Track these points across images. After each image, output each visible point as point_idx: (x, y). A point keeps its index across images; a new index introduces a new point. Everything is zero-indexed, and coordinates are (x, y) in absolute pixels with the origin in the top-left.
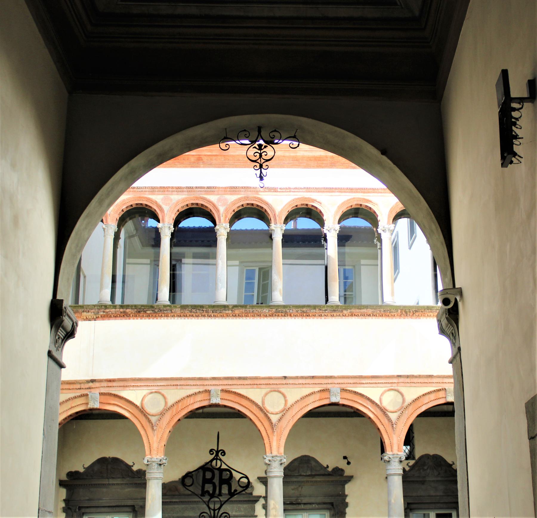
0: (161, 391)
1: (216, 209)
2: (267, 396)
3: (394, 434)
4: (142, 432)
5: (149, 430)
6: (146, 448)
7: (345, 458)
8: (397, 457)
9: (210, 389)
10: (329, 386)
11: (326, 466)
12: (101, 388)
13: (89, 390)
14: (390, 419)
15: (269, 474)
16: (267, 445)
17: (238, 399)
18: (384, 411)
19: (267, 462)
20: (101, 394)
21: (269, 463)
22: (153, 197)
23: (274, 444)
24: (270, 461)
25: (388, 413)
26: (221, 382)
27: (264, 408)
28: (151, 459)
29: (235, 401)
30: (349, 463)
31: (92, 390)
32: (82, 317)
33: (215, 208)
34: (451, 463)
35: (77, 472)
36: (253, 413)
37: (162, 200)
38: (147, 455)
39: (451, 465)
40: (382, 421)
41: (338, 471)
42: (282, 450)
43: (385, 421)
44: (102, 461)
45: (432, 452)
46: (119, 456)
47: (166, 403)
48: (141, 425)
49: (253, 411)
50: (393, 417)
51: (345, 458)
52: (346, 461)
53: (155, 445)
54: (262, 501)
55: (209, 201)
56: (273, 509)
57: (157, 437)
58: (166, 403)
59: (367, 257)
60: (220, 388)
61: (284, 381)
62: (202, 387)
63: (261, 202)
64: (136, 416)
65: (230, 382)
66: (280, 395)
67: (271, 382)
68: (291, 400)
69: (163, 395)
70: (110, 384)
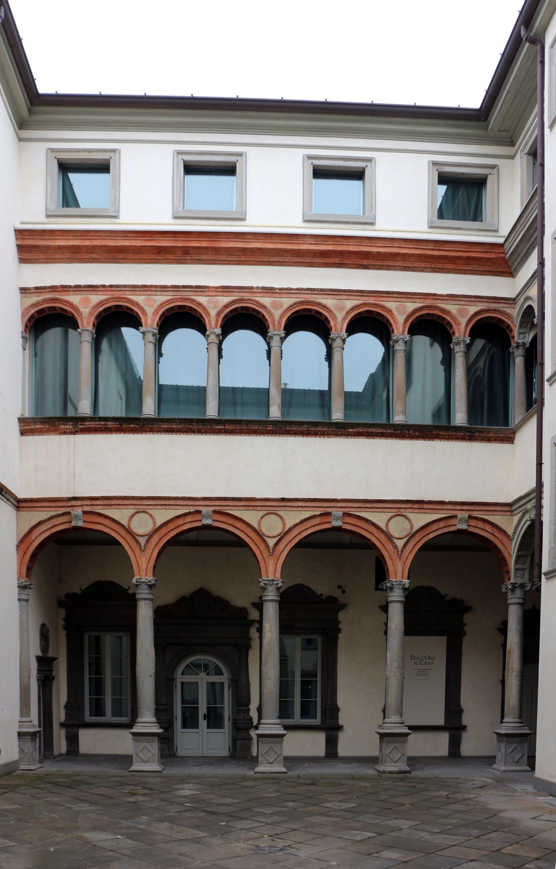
0: (148, 511)
1: (207, 312)
2: (263, 519)
3: (400, 561)
4: (130, 552)
5: (137, 550)
6: (134, 568)
7: (339, 587)
8: (400, 584)
9: (201, 510)
10: (330, 510)
11: (320, 595)
12: (84, 507)
13: (72, 508)
14: (396, 545)
15: (264, 598)
16: (263, 569)
17: (231, 521)
18: (390, 538)
19: (263, 585)
20: (84, 513)
21: (265, 587)
22: (135, 298)
23: (271, 568)
24: (265, 584)
25: (394, 540)
26: (213, 503)
27: (260, 531)
28: (140, 579)
29: (228, 523)
30: (344, 592)
31: (74, 508)
32: (60, 431)
33: (205, 311)
34: (444, 595)
35: (75, 594)
36: (248, 535)
37: (144, 301)
38: (136, 576)
39: (444, 597)
40: (387, 547)
41: (331, 600)
42: (278, 574)
43: (390, 547)
44: (99, 584)
45: (425, 584)
46: (114, 580)
47: (154, 523)
48: (128, 545)
49: (248, 534)
50: (400, 544)
51: (339, 587)
52: (341, 590)
53: (144, 566)
54: (257, 625)
55: (200, 304)
56: (268, 632)
57: (146, 558)
58: (154, 523)
59: (281, 587)
60: (213, 509)
61: (282, 504)
62: (192, 508)
63: (258, 305)
64: (123, 536)
65: (223, 503)
66: (278, 518)
67: (268, 504)
68: (289, 524)
69: (151, 515)
70: (94, 502)
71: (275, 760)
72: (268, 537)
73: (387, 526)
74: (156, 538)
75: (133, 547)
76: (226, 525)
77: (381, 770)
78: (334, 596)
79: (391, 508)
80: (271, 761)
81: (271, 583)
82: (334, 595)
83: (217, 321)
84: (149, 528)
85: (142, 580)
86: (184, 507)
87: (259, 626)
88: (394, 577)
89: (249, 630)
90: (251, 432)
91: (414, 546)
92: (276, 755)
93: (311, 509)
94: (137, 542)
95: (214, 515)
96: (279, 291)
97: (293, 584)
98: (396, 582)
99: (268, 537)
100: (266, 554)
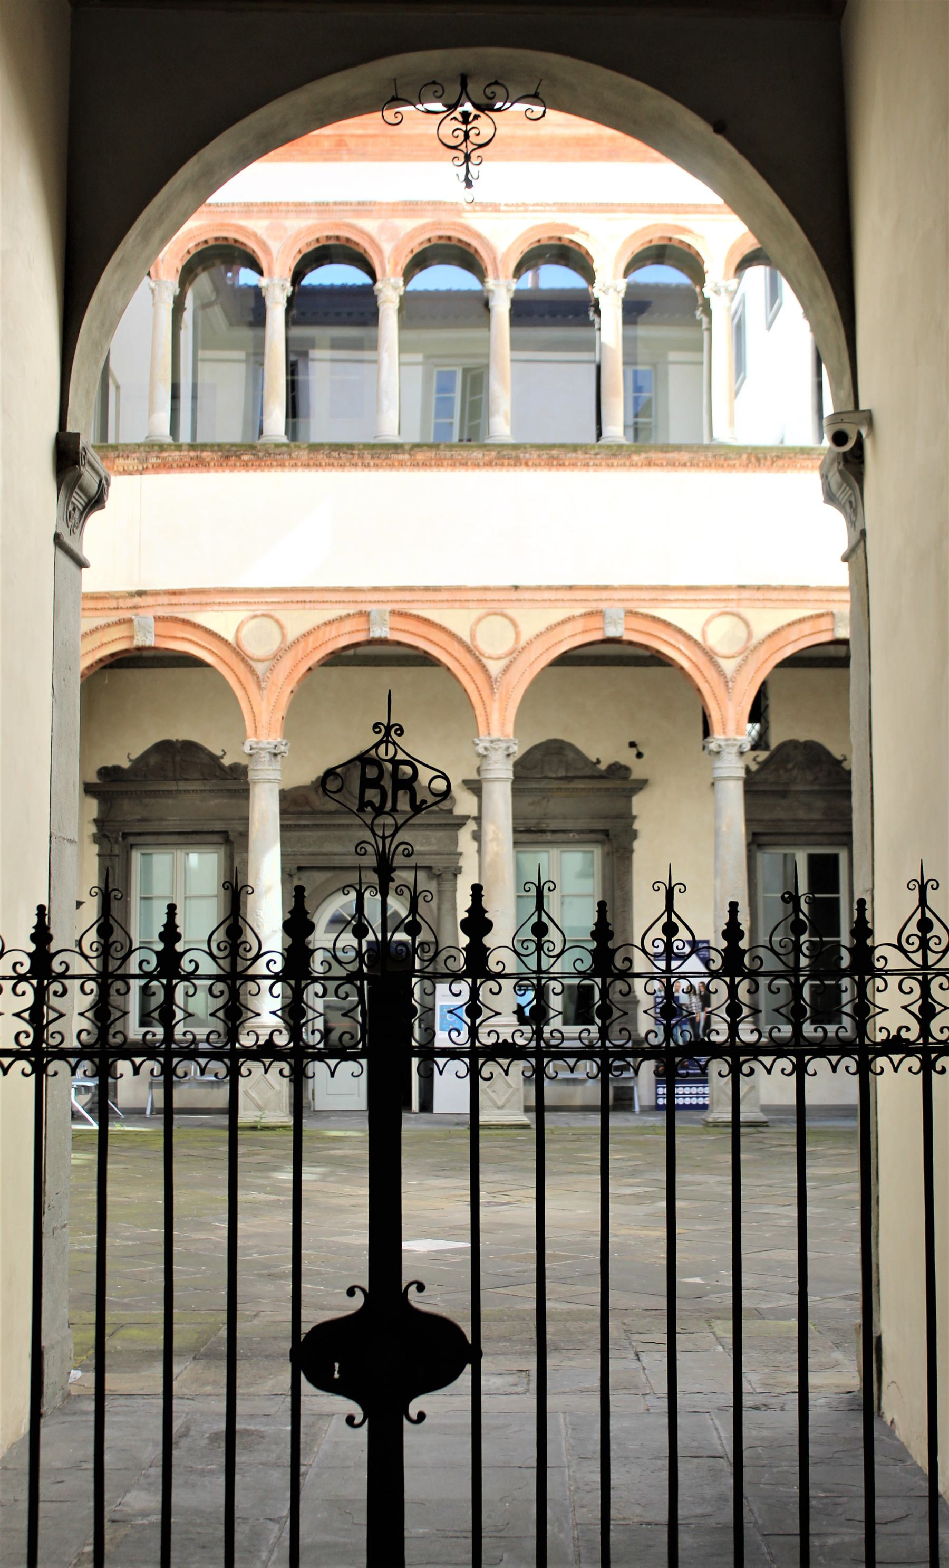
0: (272, 613)
4: (239, 693)
6: (246, 723)
7: (632, 745)
8: (734, 745)
9: (368, 610)
10: (602, 606)
13: (135, 611)
16: (481, 720)
17: (423, 629)
18: (710, 655)
19: (481, 751)
20: (158, 619)
21: (485, 753)
23: (495, 718)
24: (486, 749)
27: (475, 647)
28: (257, 743)
30: (639, 755)
31: (139, 611)
34: (840, 758)
35: (117, 769)
40: (706, 675)
41: (618, 771)
42: (510, 728)
44: (164, 747)
45: (802, 737)
47: (284, 636)
50: (729, 666)
51: (632, 745)
52: (634, 751)
54: (471, 826)
56: (492, 840)
58: (284, 636)
60: (389, 607)
62: (352, 606)
65: (408, 596)
66: (506, 622)
68: (527, 633)
69: (278, 622)
70: (174, 599)
71: (508, 1101)
72: (490, 658)
73: (704, 634)
74: (287, 663)
75: (244, 681)
76: (414, 637)
77: (710, 1120)
78: (623, 762)
79: (713, 600)
80: (500, 1103)
81: (497, 747)
82: (623, 762)
83: (396, 265)
84: (274, 644)
85: (261, 746)
86: (338, 606)
87: (100, 1125)
88: (721, 731)
89: (457, 836)
90: (457, 464)
91: (757, 671)
92: (511, 1090)
93: (567, 604)
94: (252, 671)
95: (393, 618)
96: (507, 209)
97: (543, 739)
98: (727, 740)
99: (490, 658)
100: (486, 692)
